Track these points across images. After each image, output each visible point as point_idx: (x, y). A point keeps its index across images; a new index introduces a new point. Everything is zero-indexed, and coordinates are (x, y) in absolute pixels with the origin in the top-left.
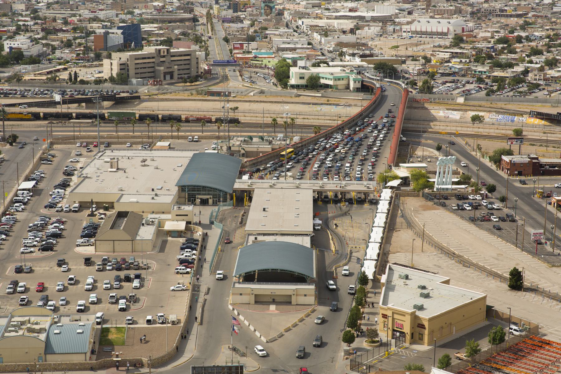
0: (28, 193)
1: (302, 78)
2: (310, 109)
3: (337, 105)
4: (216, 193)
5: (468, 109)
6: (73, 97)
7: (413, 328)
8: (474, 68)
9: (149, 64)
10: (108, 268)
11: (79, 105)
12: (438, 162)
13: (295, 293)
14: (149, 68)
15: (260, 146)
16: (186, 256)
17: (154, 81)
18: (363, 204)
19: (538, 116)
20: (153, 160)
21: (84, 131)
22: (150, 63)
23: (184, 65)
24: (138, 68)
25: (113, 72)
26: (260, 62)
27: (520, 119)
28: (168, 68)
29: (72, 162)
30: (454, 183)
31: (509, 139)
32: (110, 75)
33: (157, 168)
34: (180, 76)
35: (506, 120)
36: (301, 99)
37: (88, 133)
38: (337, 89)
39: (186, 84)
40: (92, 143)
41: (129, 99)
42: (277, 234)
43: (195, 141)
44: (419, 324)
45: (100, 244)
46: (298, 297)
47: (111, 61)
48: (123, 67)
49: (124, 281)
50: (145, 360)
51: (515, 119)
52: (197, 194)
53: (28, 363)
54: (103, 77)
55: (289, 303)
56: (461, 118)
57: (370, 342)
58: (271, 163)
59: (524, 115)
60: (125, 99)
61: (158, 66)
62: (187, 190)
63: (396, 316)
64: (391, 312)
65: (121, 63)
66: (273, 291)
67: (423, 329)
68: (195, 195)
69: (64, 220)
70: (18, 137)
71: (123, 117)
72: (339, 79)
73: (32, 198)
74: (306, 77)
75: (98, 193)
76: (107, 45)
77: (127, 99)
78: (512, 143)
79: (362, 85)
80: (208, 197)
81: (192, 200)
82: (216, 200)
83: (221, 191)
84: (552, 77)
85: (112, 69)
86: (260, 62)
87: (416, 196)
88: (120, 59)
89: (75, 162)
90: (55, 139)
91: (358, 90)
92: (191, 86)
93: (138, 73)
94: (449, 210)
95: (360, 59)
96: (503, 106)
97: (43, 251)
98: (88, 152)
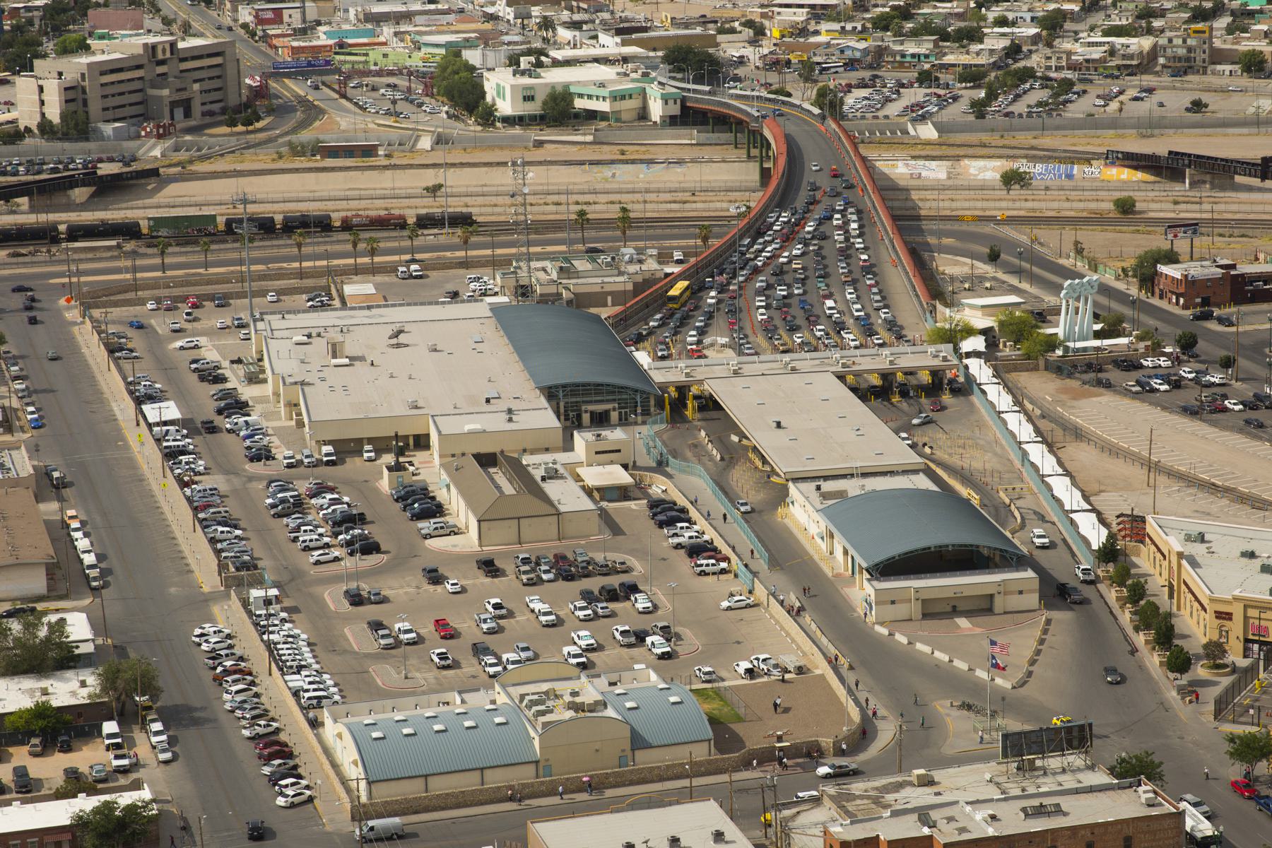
1: (529, 98)
2: (586, 178)
3: (650, 162)
5: (962, 153)
8: (898, 48)
10: (545, 577)
12: (1064, 292)
13: (1001, 589)
14: (130, 92)
15: (606, 280)
17: (158, 127)
19: (1126, 163)
22: (133, 80)
23: (210, 79)
25: (46, 110)
26: (362, 59)
27: (1086, 170)
28: (179, 90)
30: (1098, 335)
31: (1169, 227)
33: (435, 350)
35: (1055, 175)
36: (548, 152)
38: (618, 120)
39: (235, 129)
41: (132, 178)
42: (852, 475)
43: (416, 277)
45: (489, 529)
47: (41, 82)
48: (71, 95)
50: (827, 742)
51: (1075, 172)
52: (583, 402)
53: (609, 771)
56: (949, 178)
59: (1093, 162)
60: (124, 180)
61: (153, 87)
62: (561, 394)
63: (1253, 613)
64: (1242, 605)
65: (68, 85)
66: (958, 590)
71: (187, 228)
72: (623, 98)
74: (541, 97)
78: (1176, 236)
79: (684, 108)
82: (626, 413)
83: (637, 391)
84: (1087, 61)
85: (42, 103)
86: (362, 59)
87: (1032, 370)
88: (60, 74)
91: (672, 121)
92: (248, 132)
94: (1119, 393)
95: (618, 39)
96: (1034, 142)
97: (363, 553)
98: (190, 321)
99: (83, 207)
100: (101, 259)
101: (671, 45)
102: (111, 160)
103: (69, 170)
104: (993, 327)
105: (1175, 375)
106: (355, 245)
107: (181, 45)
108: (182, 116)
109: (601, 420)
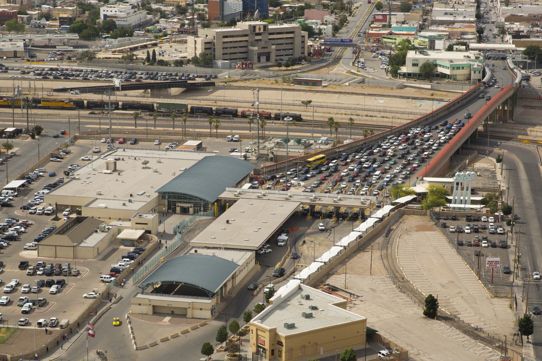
0: (12, 193)
4: (197, 202)
6: (140, 81)
7: (273, 345)
9: (241, 43)
11: (146, 91)
13: (191, 306)
14: (240, 47)
16: (120, 265)
17: (243, 64)
18: (356, 221)
20: (160, 162)
21: (120, 124)
24: (227, 48)
26: (394, 41)
29: (83, 160)
32: (193, 55)
33: (156, 172)
34: (278, 58)
37: (124, 127)
38: (455, 79)
39: (281, 68)
40: (117, 139)
42: (220, 248)
44: (278, 341)
45: (42, 249)
46: (194, 311)
47: (196, 39)
48: (208, 46)
49: (46, 286)
54: (185, 57)
55: (184, 316)
57: (232, 356)
58: (292, 170)
60: (196, 86)
63: (260, 333)
67: (282, 347)
68: (175, 202)
69: (30, 222)
70: (42, 129)
71: (173, 109)
72: (458, 68)
73: (15, 198)
74: (420, 65)
75: (74, 196)
76: (223, 14)
77: (198, 86)
80: (188, 205)
81: (173, 208)
82: (197, 209)
87: (423, 215)
88: (207, 36)
89: (87, 160)
90: (82, 132)
93: (227, 54)
99: (175, 97)
100: (125, 119)
101: (529, 45)
102: (201, 77)
103: (181, 79)
104: (427, 192)
105: (476, 226)
106: (211, 123)
107: (271, 27)
108: (265, 60)
109: (185, 211)
